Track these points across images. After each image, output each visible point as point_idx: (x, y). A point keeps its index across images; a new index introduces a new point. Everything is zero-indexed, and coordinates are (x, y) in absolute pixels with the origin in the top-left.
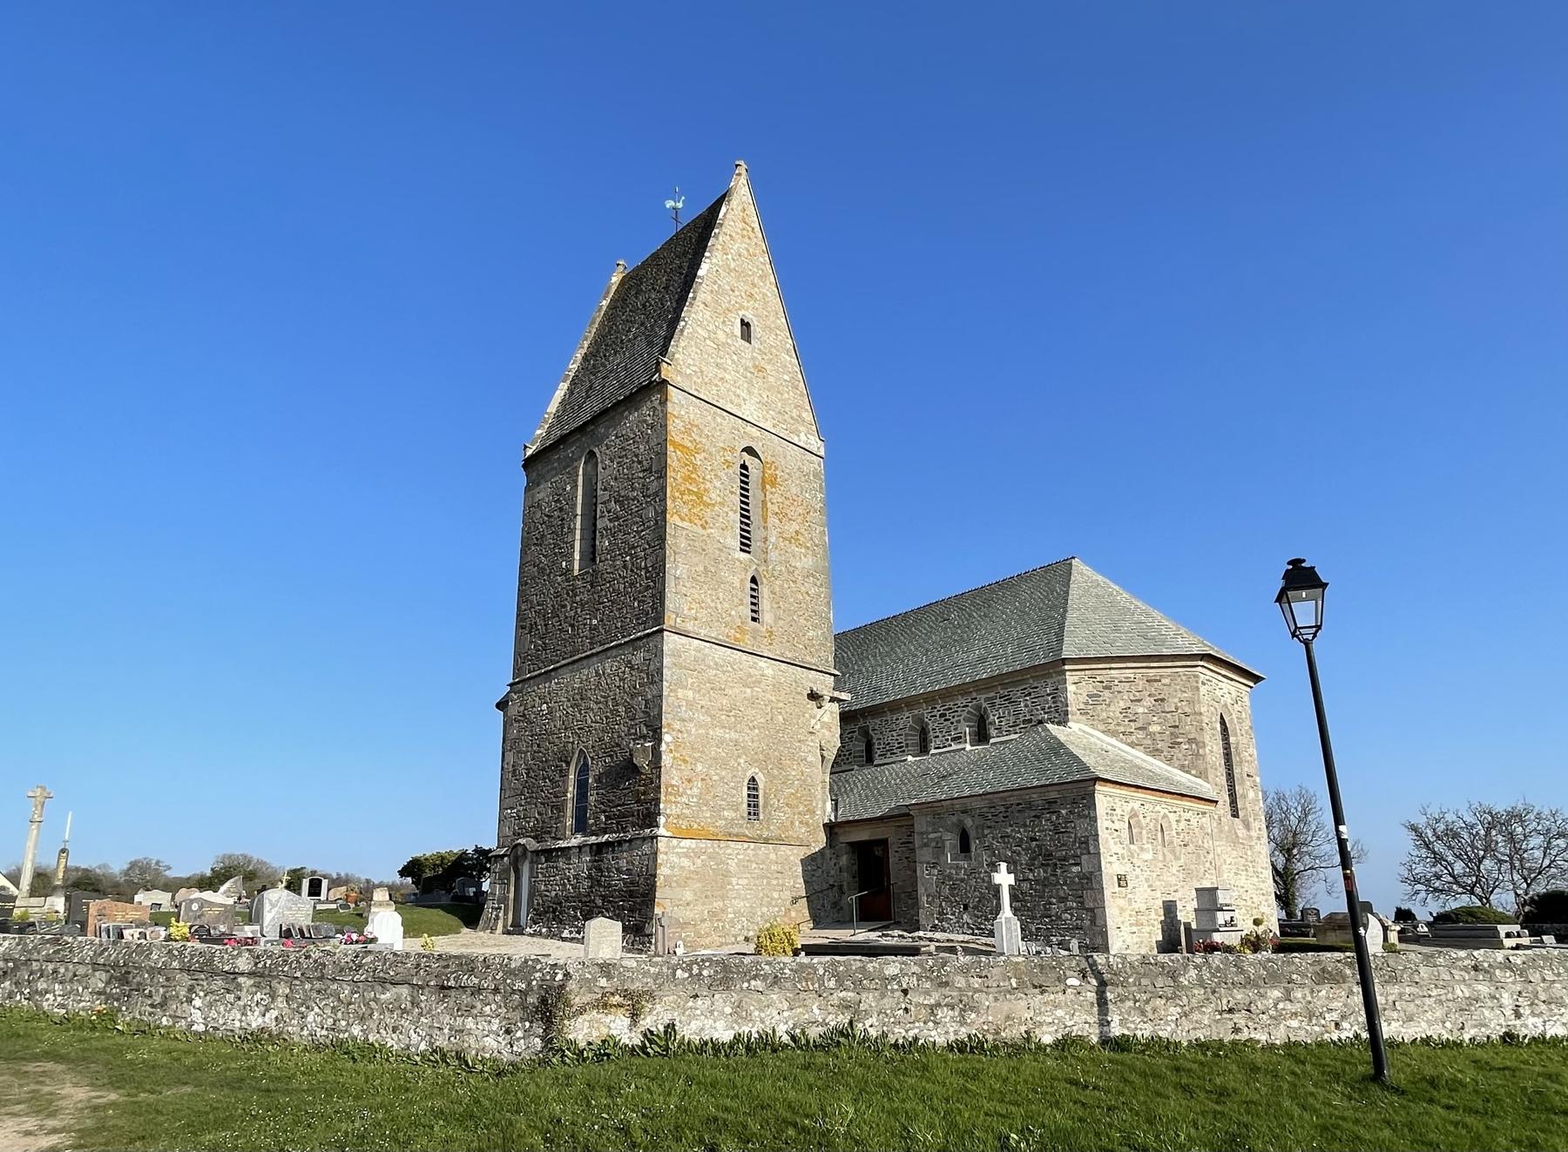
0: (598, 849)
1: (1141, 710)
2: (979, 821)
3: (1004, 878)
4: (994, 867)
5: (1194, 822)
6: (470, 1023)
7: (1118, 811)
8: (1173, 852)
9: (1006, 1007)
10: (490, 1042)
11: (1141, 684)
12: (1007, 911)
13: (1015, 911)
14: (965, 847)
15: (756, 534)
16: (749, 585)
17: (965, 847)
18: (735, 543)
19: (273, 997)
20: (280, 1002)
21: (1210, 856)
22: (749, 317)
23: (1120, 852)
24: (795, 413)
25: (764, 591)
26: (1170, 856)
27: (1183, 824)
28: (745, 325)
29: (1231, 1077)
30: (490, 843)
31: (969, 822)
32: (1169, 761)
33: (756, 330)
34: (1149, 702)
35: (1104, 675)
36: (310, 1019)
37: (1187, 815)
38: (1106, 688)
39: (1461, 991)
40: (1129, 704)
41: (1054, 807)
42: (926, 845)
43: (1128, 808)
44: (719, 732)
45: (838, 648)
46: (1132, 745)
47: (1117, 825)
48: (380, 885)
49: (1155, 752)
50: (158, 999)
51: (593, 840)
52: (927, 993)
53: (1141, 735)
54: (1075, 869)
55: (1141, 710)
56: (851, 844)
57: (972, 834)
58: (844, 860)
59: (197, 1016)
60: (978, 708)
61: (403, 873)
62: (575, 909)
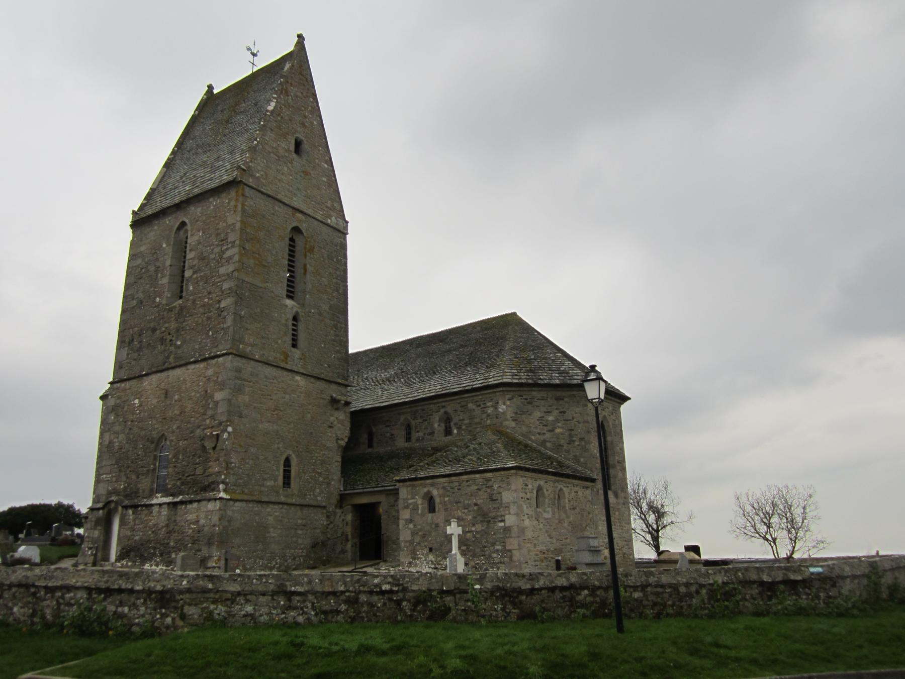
0: (175, 504)
2: (441, 491)
3: (454, 529)
5: (580, 493)
7: (530, 486)
8: (565, 513)
12: (455, 550)
13: (463, 553)
14: (432, 509)
15: (299, 286)
16: (290, 322)
17: (432, 509)
18: (282, 290)
21: (591, 516)
22: (301, 137)
23: (530, 513)
24: (329, 204)
25: (301, 326)
26: (564, 516)
27: (573, 494)
28: (298, 144)
30: (83, 504)
33: (305, 146)
34: (556, 413)
37: (576, 489)
38: (529, 403)
40: (542, 415)
41: (490, 483)
42: (406, 507)
43: (536, 484)
44: (266, 425)
45: (351, 418)
47: (529, 495)
48: (605, 382)
54: (502, 524)
57: (437, 500)
58: (349, 517)
62: (155, 548)
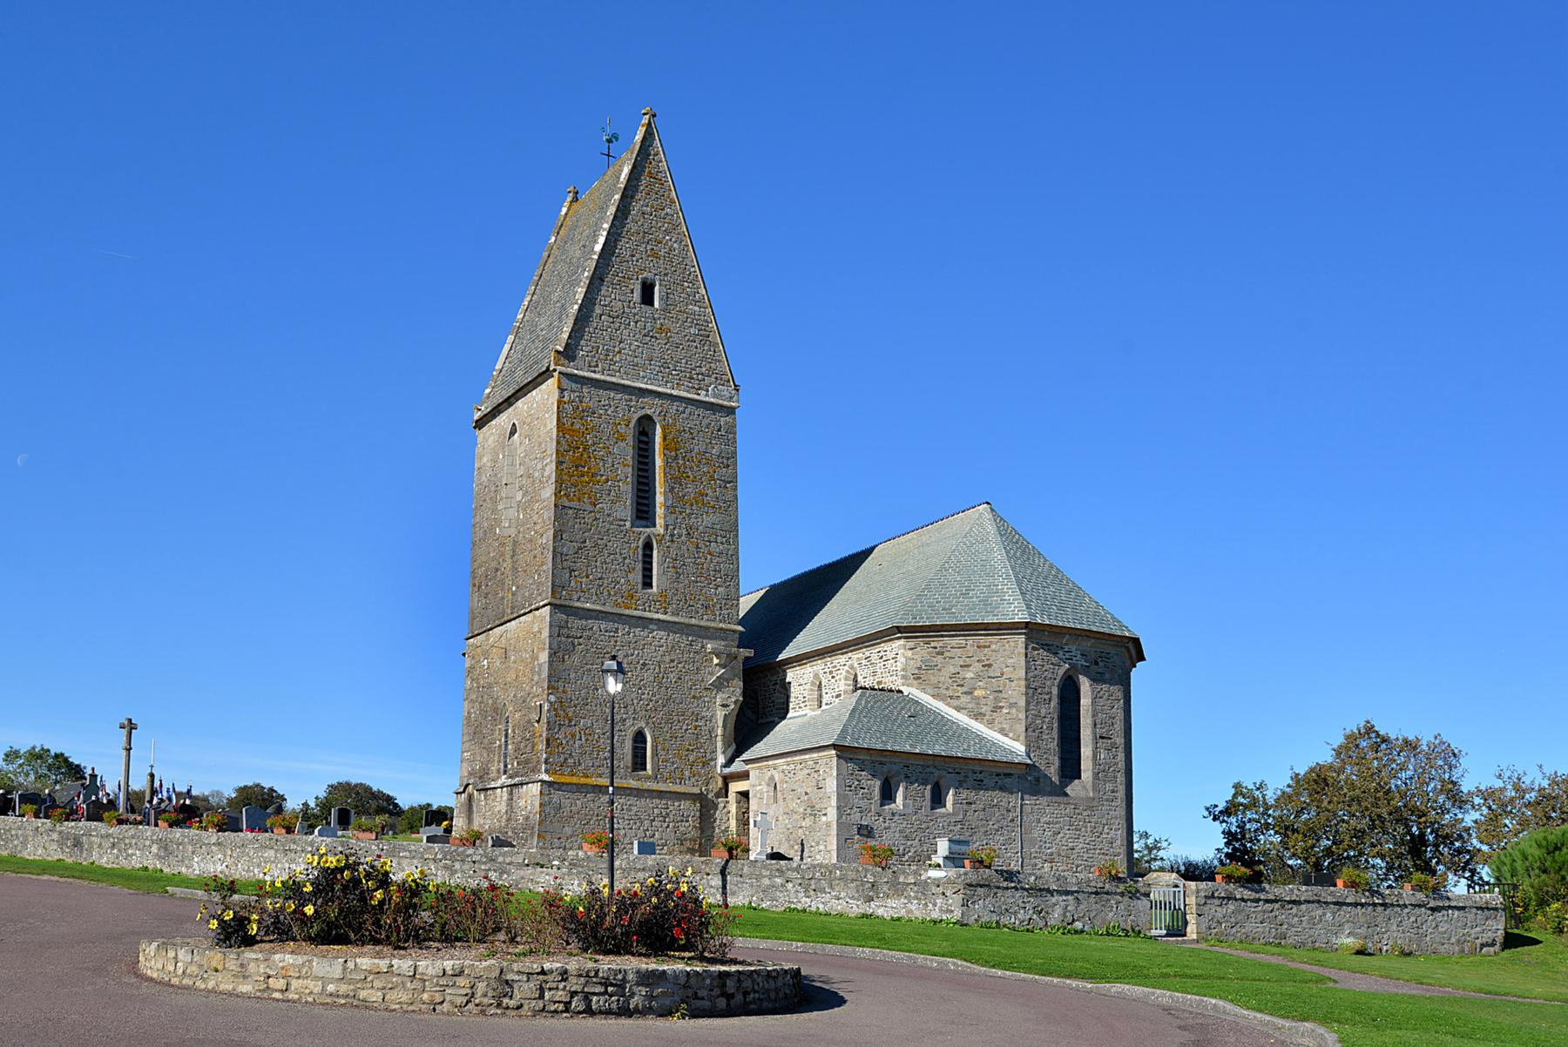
9: (521, 873)
11: (971, 650)
29: (569, 548)
32: (990, 724)
35: (938, 643)
39: (766, 882)
46: (958, 709)
49: (978, 716)
53: (965, 699)
60: (852, 667)
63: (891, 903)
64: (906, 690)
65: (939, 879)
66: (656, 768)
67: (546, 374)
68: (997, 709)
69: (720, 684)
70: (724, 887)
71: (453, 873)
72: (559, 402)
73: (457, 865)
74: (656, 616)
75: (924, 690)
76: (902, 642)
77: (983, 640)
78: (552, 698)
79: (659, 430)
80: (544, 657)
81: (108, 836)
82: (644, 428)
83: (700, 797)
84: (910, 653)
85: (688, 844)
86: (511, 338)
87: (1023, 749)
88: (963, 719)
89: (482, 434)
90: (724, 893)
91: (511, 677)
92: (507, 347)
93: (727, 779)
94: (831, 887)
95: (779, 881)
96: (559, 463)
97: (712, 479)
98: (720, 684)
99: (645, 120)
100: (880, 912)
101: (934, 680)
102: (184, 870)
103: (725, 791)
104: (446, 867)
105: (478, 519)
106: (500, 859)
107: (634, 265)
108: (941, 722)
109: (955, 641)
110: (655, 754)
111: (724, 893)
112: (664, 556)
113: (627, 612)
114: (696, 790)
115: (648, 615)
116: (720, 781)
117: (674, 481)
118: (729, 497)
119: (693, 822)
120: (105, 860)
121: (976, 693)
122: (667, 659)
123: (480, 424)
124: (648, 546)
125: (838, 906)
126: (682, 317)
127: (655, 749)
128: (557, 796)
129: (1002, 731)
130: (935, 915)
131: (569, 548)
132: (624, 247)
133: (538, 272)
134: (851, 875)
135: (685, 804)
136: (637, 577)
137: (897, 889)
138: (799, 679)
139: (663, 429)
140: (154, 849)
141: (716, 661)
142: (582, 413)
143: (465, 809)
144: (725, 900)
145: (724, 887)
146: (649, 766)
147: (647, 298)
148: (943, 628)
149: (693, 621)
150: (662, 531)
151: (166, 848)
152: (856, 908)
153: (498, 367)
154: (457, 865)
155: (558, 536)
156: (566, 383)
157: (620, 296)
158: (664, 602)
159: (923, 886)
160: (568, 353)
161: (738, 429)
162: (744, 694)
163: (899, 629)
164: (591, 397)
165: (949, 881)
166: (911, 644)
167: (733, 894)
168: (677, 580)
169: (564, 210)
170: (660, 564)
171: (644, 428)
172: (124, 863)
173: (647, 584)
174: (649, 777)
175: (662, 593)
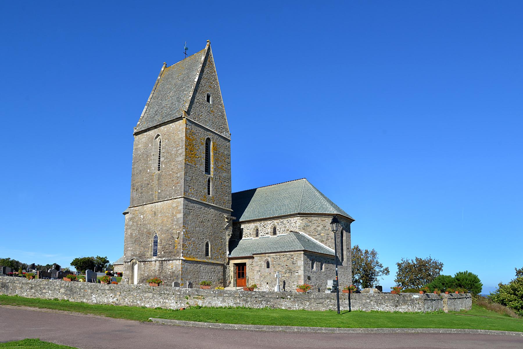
1: (319, 229)
4: (330, 279)
6: (167, 301)
9: (275, 301)
10: (172, 305)
11: (320, 221)
19: (115, 295)
20: (118, 296)
29: (188, 179)
31: (269, 260)
32: (326, 244)
35: (310, 219)
36: (126, 300)
39: (364, 301)
41: (293, 257)
46: (316, 239)
49: (322, 242)
50: (82, 295)
51: (160, 259)
52: (260, 298)
53: (318, 236)
54: (297, 274)
55: (319, 229)
56: (235, 264)
57: (270, 263)
59: (94, 299)
60: (274, 224)
61: (72, 264)
63: (403, 307)
64: (301, 233)
65: (416, 298)
66: (212, 255)
67: (181, 118)
68: (328, 239)
69: (227, 228)
70: (350, 304)
71: (247, 302)
72: (186, 129)
73: (249, 299)
74: (212, 204)
75: (306, 233)
76: (299, 218)
77: (323, 219)
78: (184, 230)
79: (211, 142)
80: (180, 216)
81: (27, 284)
82: (208, 140)
83: (222, 265)
84: (301, 221)
85: (220, 281)
86: (146, 107)
87: (334, 251)
88: (318, 242)
89: (137, 138)
90: (350, 306)
91: (159, 221)
92: (145, 110)
93: (230, 259)
94: (385, 302)
95: (368, 301)
96: (186, 149)
97: (225, 161)
98: (227, 228)
99: (208, 43)
100: (400, 310)
101: (309, 230)
102: (85, 301)
103: (228, 263)
104: (244, 300)
105: (136, 166)
106: (267, 296)
107: (205, 88)
108: (315, 245)
109: (315, 218)
110: (211, 250)
111: (350, 306)
112: (213, 185)
113: (204, 202)
114: (222, 263)
115: (209, 203)
116: (228, 259)
117: (216, 161)
118: (229, 168)
119: (221, 273)
120: (26, 294)
121: (322, 234)
122: (214, 219)
123: (137, 134)
124: (209, 181)
125: (387, 309)
126: (217, 108)
127: (211, 248)
128: (186, 265)
129: (329, 246)
130: (416, 310)
131: (188, 179)
132: (203, 82)
133: (154, 87)
134: (391, 298)
135: (219, 267)
136: (206, 191)
137: (405, 302)
138: (247, 229)
139: (213, 143)
140: (62, 290)
141: (226, 220)
142: (193, 134)
143: (131, 268)
144: (350, 309)
145: (350, 304)
146: (209, 255)
147: (208, 100)
148: (325, 214)
149: (221, 207)
150: (213, 176)
151: (71, 291)
152: (392, 309)
153: (142, 115)
154: (249, 299)
155: (186, 173)
156: (188, 122)
157: (201, 98)
158: (210, 199)
159: (413, 300)
160: (188, 113)
161: (231, 147)
162: (233, 231)
163: (299, 214)
164: (195, 129)
165: (420, 299)
166: (302, 219)
167: (353, 306)
168: (216, 193)
169: (162, 69)
170: (212, 187)
171: (208, 140)
172: (40, 296)
173: (209, 194)
174: (210, 258)
175: (213, 196)
